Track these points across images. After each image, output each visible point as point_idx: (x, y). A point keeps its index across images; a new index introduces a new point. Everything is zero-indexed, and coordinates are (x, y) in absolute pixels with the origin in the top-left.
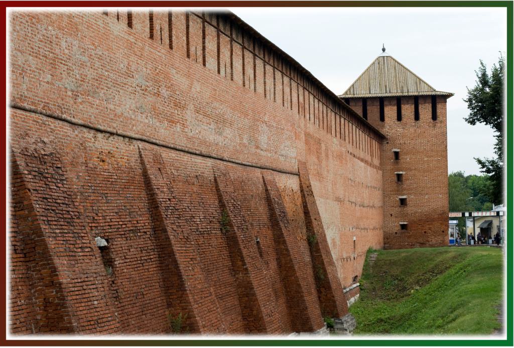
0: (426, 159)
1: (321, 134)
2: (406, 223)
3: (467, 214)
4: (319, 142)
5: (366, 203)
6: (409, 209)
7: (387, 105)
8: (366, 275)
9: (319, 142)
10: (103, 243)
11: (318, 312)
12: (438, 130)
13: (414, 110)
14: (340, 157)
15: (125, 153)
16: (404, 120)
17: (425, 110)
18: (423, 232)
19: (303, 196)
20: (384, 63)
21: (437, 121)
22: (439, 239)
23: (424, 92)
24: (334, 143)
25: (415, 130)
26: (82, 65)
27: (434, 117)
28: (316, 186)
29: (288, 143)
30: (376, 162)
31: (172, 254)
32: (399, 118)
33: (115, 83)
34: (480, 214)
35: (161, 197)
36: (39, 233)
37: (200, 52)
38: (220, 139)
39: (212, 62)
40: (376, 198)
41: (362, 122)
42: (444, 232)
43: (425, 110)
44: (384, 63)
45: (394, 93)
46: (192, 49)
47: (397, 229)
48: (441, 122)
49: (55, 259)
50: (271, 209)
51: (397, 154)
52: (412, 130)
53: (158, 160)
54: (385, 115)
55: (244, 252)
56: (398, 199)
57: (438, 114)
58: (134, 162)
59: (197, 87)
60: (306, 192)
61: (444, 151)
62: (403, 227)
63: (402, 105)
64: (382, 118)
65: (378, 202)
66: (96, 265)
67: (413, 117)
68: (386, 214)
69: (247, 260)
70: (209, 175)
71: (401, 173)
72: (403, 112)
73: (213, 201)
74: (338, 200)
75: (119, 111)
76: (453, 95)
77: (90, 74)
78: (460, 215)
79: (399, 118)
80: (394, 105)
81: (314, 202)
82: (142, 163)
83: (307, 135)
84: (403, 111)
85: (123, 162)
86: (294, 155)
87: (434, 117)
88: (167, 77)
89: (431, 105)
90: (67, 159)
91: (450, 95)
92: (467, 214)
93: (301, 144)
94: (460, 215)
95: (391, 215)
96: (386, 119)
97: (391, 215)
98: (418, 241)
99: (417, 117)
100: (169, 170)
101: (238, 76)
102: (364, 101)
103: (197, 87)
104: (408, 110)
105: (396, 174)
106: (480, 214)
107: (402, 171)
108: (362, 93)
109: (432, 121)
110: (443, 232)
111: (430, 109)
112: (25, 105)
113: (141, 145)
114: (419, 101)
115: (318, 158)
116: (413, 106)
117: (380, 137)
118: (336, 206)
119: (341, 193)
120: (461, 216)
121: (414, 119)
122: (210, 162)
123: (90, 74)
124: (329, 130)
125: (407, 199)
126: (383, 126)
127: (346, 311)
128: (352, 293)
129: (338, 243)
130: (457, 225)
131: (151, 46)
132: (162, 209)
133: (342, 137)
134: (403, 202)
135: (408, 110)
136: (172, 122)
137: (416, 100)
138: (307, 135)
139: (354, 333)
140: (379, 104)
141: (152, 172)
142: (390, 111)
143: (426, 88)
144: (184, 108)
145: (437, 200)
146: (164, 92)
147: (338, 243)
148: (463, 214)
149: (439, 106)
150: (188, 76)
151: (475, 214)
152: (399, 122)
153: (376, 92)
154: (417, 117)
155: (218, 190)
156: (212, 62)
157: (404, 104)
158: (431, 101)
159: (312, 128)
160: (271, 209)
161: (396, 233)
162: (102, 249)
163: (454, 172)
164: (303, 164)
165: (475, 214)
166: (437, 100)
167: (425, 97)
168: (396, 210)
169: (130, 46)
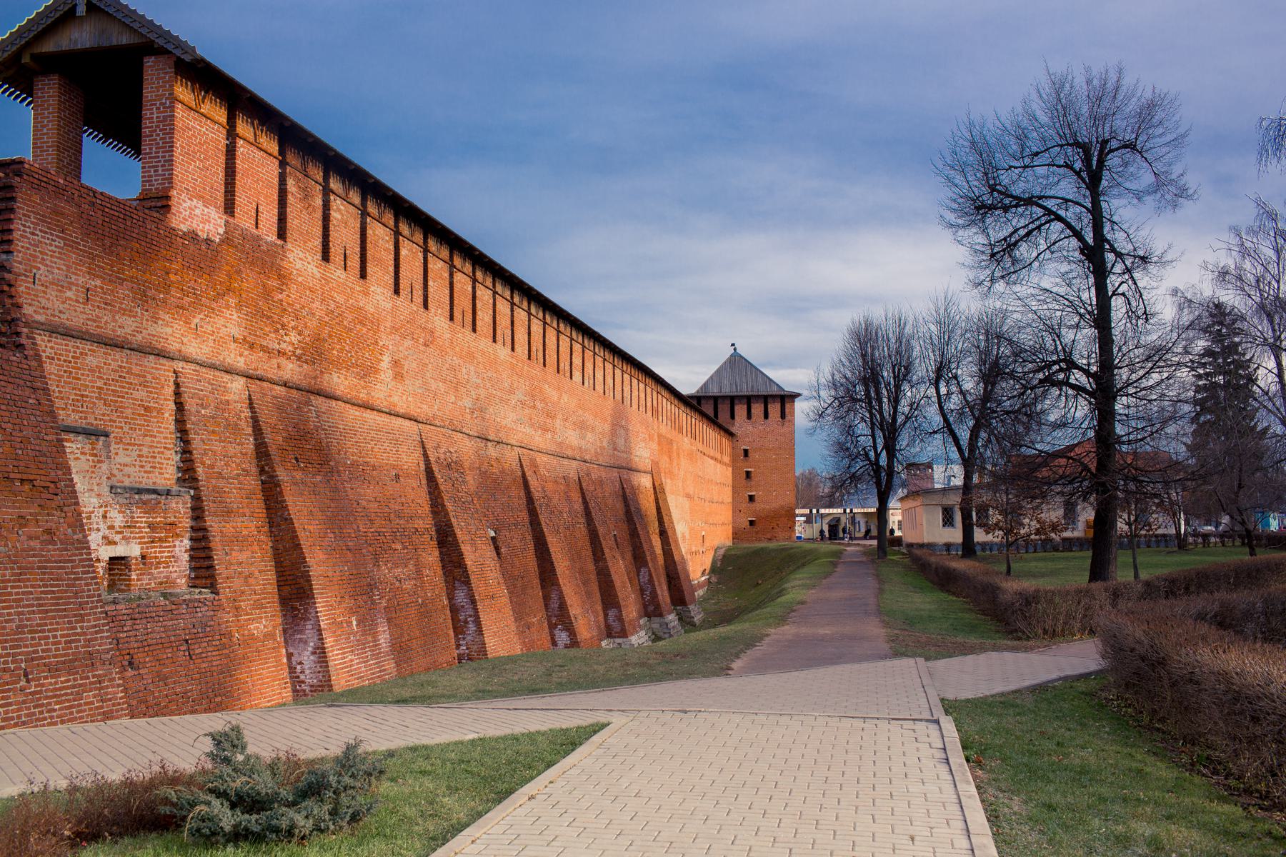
1: (672, 434)
3: (814, 511)
4: (670, 442)
5: (715, 499)
6: (758, 506)
8: (714, 570)
9: (670, 442)
10: (493, 534)
11: (668, 599)
14: (690, 456)
15: (510, 457)
16: (754, 418)
17: (774, 409)
19: (655, 493)
20: (736, 362)
22: (787, 535)
23: (774, 391)
24: (686, 442)
26: (477, 386)
27: (783, 416)
28: (668, 485)
29: (643, 445)
30: (727, 459)
31: (545, 544)
33: (502, 400)
34: (827, 511)
35: (536, 495)
36: (450, 525)
37: (568, 368)
38: (583, 443)
39: (577, 376)
40: (727, 495)
41: (713, 421)
42: (792, 528)
43: (774, 409)
44: (736, 362)
45: (745, 391)
46: (562, 365)
50: (627, 505)
51: (746, 452)
53: (534, 464)
55: (604, 543)
58: (515, 464)
59: (565, 398)
60: (658, 491)
62: (752, 523)
64: (733, 417)
65: (730, 481)
66: (489, 553)
68: (736, 511)
69: (606, 551)
70: (573, 475)
73: (576, 497)
74: (688, 496)
75: (503, 424)
77: (483, 394)
78: (807, 511)
81: (666, 499)
82: (522, 466)
83: (660, 436)
85: (507, 466)
86: (647, 455)
87: (783, 416)
88: (541, 392)
90: (466, 465)
91: (799, 395)
92: (814, 511)
93: (655, 446)
94: (807, 511)
99: (766, 416)
100: (542, 471)
101: (599, 387)
102: (716, 399)
103: (565, 398)
104: (757, 409)
106: (827, 511)
108: (714, 391)
112: (437, 422)
113: (521, 451)
115: (670, 457)
117: (730, 434)
118: (686, 503)
119: (691, 490)
122: (575, 464)
123: (483, 394)
124: (680, 430)
127: (693, 601)
128: (700, 586)
129: (687, 536)
131: (529, 366)
132: (537, 505)
133: (693, 436)
134: (751, 498)
135: (757, 409)
136: (546, 430)
137: (766, 399)
138: (660, 436)
141: (529, 474)
142: (740, 410)
143: (776, 388)
144: (553, 418)
145: (785, 497)
146: (539, 405)
147: (687, 536)
149: (787, 406)
150: (558, 389)
151: (822, 511)
153: (727, 390)
154: (766, 416)
155: (581, 489)
156: (577, 376)
159: (665, 429)
160: (627, 505)
162: (493, 538)
163: (1096, 70)
164: (655, 463)
165: (822, 511)
166: (786, 399)
167: (774, 397)
168: (745, 505)
169: (513, 367)
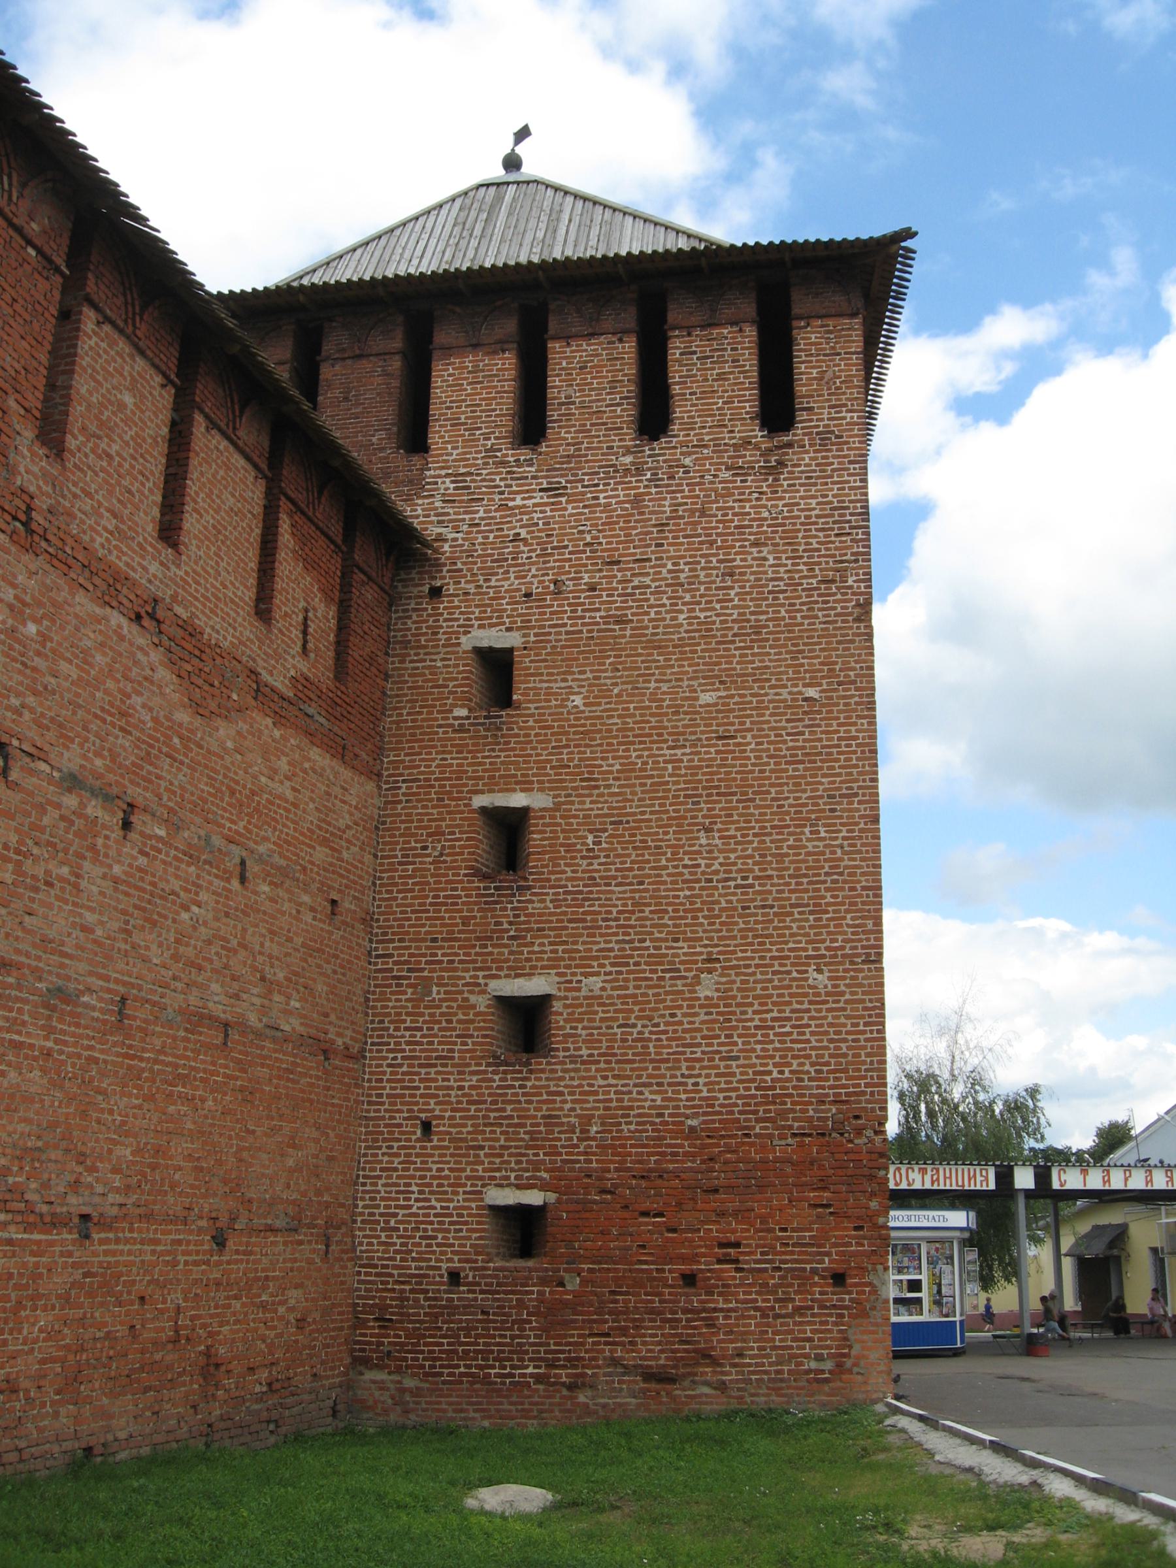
0: (706, 698)
2: (534, 1198)
6: (571, 1086)
7: (448, 350)
12: (800, 496)
13: (631, 370)
16: (562, 433)
18: (671, 1273)
21: (798, 433)
25: (637, 501)
27: (777, 408)
32: (532, 425)
43: (715, 369)
47: (464, 1241)
48: (825, 439)
49: (1164, 1535)
52: (613, 495)
54: (434, 410)
56: (481, 1002)
57: (801, 389)
61: (858, 620)
62: (523, 1229)
63: (554, 346)
64: (415, 435)
67: (625, 413)
71: (518, 800)
72: (557, 386)
76: (916, 234)
79: (532, 425)
80: (499, 347)
84: (555, 382)
87: (777, 408)
89: (751, 332)
94: (985, 1179)
95: (427, 1127)
96: (438, 435)
97: (427, 1127)
98: (630, 1358)
105: (484, 810)
107: (526, 786)
109: (758, 434)
110: (839, 1279)
111: (749, 361)
114: (672, 316)
116: (628, 348)
120: (992, 1186)
121: (629, 432)
125: (557, 1006)
126: (417, 485)
130: (972, 1239)
135: (592, 371)
139: (933, 1455)
140: (397, 343)
142: (472, 387)
148: (1005, 1177)
152: (525, 454)
154: (654, 415)
157: (567, 338)
158: (750, 309)
161: (455, 1277)
